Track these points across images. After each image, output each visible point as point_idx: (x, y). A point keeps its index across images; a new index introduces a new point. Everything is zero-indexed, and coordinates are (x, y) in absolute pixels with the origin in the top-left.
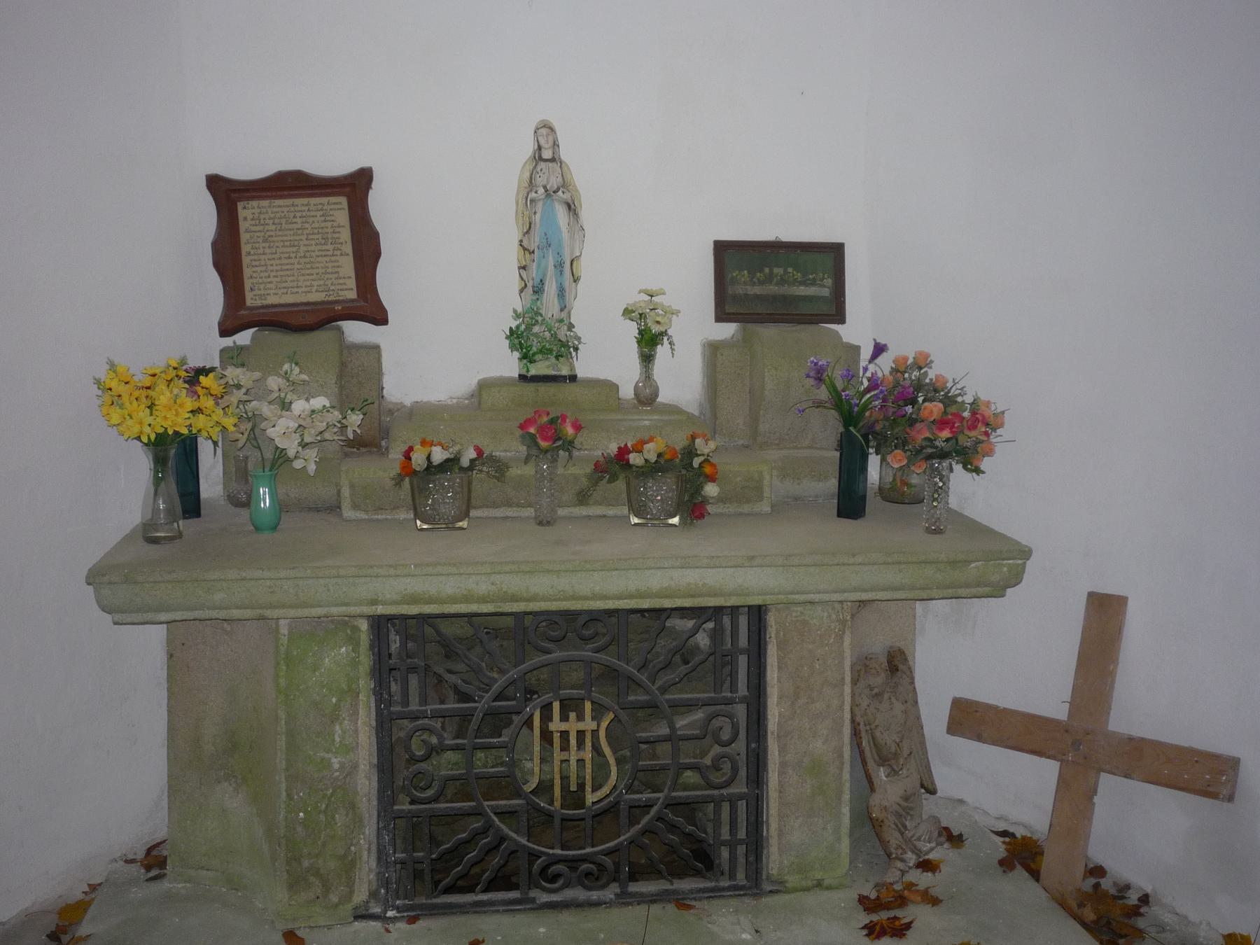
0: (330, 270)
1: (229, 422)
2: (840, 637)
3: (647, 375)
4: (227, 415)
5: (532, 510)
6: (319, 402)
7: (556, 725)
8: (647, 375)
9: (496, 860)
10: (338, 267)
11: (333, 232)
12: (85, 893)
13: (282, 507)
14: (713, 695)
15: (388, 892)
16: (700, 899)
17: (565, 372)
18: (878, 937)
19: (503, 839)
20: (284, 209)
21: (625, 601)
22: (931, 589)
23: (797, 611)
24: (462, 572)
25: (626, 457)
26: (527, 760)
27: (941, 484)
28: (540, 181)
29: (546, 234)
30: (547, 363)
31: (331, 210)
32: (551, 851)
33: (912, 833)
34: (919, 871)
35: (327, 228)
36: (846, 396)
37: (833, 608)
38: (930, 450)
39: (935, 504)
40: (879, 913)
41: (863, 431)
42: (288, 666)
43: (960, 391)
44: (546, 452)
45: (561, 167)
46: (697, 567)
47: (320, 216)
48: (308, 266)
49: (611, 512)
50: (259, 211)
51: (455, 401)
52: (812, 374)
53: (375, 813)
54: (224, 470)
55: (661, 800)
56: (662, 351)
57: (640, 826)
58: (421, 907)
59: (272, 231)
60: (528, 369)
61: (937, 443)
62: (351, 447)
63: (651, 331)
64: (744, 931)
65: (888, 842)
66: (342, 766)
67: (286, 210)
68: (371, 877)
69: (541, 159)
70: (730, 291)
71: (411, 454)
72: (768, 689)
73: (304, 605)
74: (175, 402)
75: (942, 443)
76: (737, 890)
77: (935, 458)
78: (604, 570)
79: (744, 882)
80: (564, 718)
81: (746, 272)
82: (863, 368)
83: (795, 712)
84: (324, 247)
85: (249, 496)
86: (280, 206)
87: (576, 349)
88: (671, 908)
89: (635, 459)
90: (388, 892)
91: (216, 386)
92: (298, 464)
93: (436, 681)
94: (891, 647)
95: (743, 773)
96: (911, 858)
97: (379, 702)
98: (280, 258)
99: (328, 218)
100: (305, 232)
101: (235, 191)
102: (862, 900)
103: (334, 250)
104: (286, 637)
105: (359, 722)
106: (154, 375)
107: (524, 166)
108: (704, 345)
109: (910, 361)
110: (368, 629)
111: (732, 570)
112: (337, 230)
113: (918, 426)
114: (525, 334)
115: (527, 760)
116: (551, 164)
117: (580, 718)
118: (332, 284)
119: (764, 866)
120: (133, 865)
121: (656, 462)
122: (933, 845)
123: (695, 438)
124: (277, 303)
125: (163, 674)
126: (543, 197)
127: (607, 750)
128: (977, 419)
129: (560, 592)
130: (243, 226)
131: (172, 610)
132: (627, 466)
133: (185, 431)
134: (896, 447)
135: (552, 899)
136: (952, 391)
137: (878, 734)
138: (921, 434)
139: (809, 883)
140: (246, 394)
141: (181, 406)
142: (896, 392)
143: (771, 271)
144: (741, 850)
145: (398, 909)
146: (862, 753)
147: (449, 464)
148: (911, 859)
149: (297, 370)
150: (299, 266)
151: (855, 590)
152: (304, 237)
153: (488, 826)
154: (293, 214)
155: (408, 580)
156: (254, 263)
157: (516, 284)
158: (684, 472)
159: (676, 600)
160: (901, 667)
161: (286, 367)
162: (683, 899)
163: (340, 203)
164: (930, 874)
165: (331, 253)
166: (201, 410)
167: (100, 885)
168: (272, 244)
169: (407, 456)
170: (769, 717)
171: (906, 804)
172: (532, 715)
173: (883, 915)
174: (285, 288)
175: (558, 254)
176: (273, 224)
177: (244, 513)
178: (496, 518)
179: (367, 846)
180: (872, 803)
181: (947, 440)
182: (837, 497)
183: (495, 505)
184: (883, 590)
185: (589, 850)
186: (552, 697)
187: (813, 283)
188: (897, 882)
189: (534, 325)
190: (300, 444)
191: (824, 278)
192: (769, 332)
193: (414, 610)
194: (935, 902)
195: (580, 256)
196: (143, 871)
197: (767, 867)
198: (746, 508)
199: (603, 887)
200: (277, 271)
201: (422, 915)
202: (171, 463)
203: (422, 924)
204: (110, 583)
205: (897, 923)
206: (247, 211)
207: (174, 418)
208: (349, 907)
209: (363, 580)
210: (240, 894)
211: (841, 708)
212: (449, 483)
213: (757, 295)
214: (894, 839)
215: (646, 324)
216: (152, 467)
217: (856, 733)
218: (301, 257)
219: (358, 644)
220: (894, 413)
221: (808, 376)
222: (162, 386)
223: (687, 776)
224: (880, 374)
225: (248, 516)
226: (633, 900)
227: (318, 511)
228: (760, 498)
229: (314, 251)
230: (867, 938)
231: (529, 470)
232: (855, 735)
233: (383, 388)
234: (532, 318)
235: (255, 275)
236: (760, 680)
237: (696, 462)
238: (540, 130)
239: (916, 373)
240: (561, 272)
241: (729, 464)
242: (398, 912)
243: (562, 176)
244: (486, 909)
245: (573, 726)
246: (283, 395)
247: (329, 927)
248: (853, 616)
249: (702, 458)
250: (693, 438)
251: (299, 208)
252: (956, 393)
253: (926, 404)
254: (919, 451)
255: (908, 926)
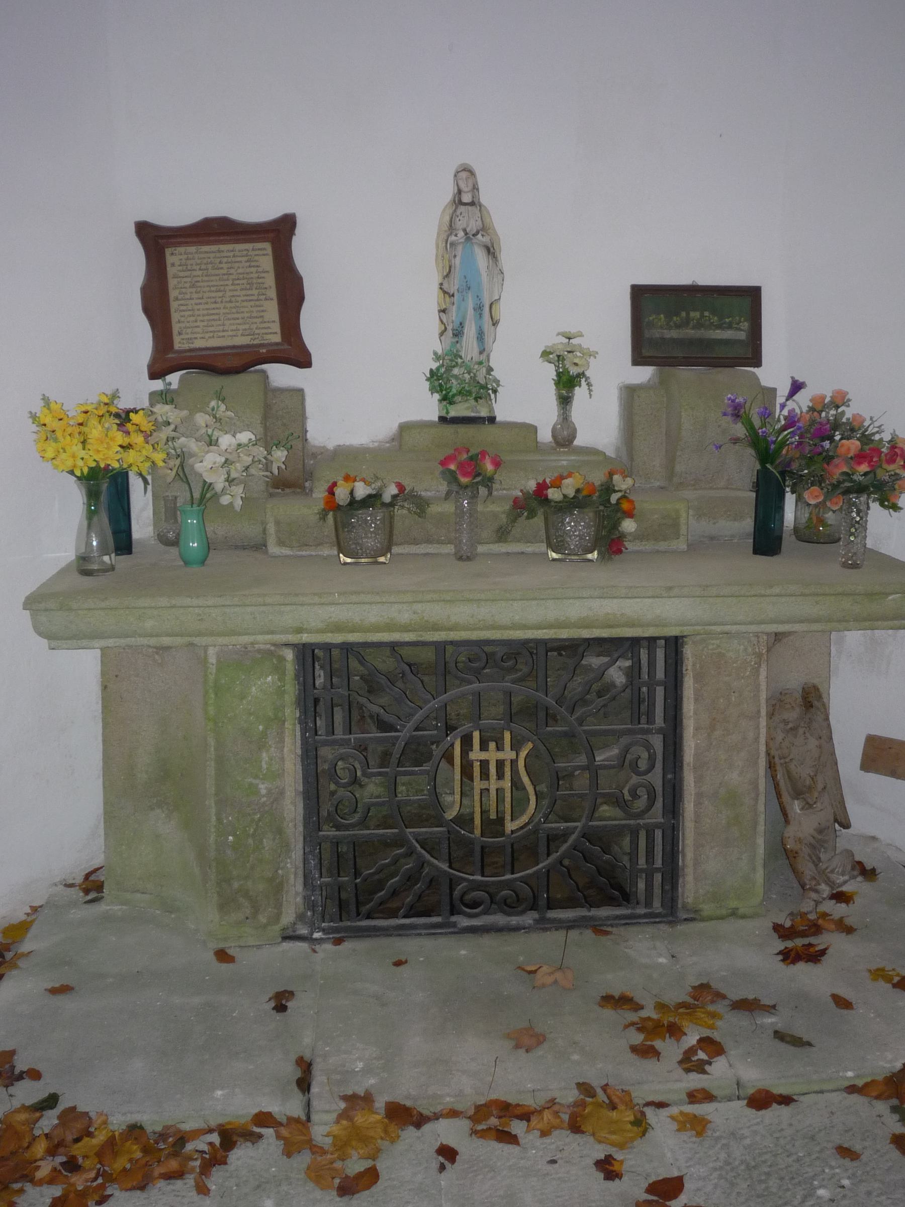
0: (255, 314)
1: (159, 457)
2: (756, 671)
3: (565, 416)
4: (156, 450)
5: (452, 547)
6: (245, 437)
7: (476, 755)
8: (565, 416)
9: (418, 885)
10: (263, 311)
11: (258, 278)
12: (28, 914)
13: (209, 546)
14: (630, 726)
15: (314, 915)
16: (617, 925)
17: (484, 413)
18: (794, 962)
19: (422, 864)
20: (209, 255)
21: (544, 631)
22: (847, 621)
23: (713, 644)
24: (384, 600)
25: (545, 492)
26: (447, 793)
27: (858, 519)
28: (460, 224)
29: (465, 277)
30: (467, 405)
31: (256, 255)
32: (471, 878)
33: (826, 865)
34: (834, 901)
35: (252, 273)
36: (763, 432)
37: (750, 641)
38: (848, 484)
39: (852, 539)
40: (794, 941)
41: (780, 469)
42: (216, 694)
43: (877, 429)
44: (466, 487)
45: (480, 210)
46: (615, 598)
47: (246, 262)
48: (234, 310)
49: (530, 548)
50: (186, 256)
51: (376, 444)
52: (730, 410)
53: (301, 838)
54: (154, 510)
55: (578, 829)
56: (580, 393)
57: (558, 854)
58: (345, 929)
59: (198, 276)
60: (447, 410)
61: (855, 477)
62: (275, 488)
63: (569, 372)
64: (660, 955)
65: (802, 873)
66: (269, 791)
67: (212, 255)
68: (298, 899)
69: (461, 203)
70: (647, 334)
71: (335, 489)
72: (685, 721)
73: (233, 633)
74: (107, 435)
75: (861, 478)
76: (653, 918)
77: (852, 493)
78: (523, 600)
79: (660, 910)
80: (484, 747)
81: (662, 316)
82: (781, 405)
83: (711, 744)
84: (250, 292)
85: (178, 536)
86: (206, 252)
87: (495, 391)
88: (588, 934)
89: (554, 494)
90: (314, 915)
91: (146, 422)
92: (225, 500)
93: (359, 717)
94: (806, 684)
95: (659, 804)
96: (825, 890)
97: (304, 731)
98: (207, 303)
99: (253, 264)
100: (231, 277)
101: (163, 237)
102: (777, 928)
103: (259, 295)
104: (214, 667)
105: (286, 750)
106: (86, 412)
107: (444, 210)
108: (621, 389)
109: (827, 400)
110: (293, 659)
111: (650, 600)
112: (263, 275)
113: (836, 461)
114: (445, 376)
115: (447, 793)
116: (470, 208)
117: (499, 748)
118: (256, 328)
119: (680, 894)
120: (72, 889)
121: (574, 497)
122: (846, 878)
123: (613, 475)
124: (203, 346)
125: (97, 708)
126: (463, 240)
127: (526, 780)
128: (896, 454)
129: (480, 621)
130: (171, 271)
131: (106, 638)
132: (546, 501)
133: (116, 465)
134: (813, 484)
135: (472, 924)
136: (870, 429)
137: (792, 767)
138: (838, 470)
139: (724, 912)
140: (175, 430)
141: (113, 439)
142: (812, 430)
143: (688, 314)
144: (658, 877)
145: (323, 930)
146: (776, 786)
147: (372, 499)
148: (824, 890)
149: (223, 407)
150: (225, 311)
151: (772, 621)
152: (230, 282)
153: (411, 853)
154: (219, 260)
155: (332, 609)
156: (182, 308)
157: (436, 327)
158: (601, 508)
159: (594, 630)
160: (816, 703)
161: (213, 403)
162: (601, 925)
163: (264, 249)
164: (843, 905)
165: (255, 298)
166: (131, 446)
167: (40, 907)
168: (199, 289)
169: (331, 492)
170: (685, 748)
171: (820, 837)
172: (452, 745)
173: (799, 942)
174: (211, 332)
175: (478, 296)
176: (200, 269)
177: (174, 551)
178: (418, 555)
179: (293, 870)
180: (786, 835)
181: (865, 474)
182: (752, 537)
183: (415, 542)
184: (801, 622)
185: (508, 876)
186: (472, 726)
187: (730, 327)
188: (811, 912)
189: (454, 367)
190: (227, 480)
191: (740, 322)
192: (685, 373)
193: (338, 638)
194: (849, 930)
195: (499, 299)
196: (82, 894)
197: (683, 896)
198: (662, 546)
199: (523, 912)
200: (204, 315)
201: (346, 937)
202: (103, 498)
203: (347, 945)
204: (46, 610)
205: (811, 950)
206: (175, 258)
207: (106, 451)
208: (277, 928)
209: (288, 608)
210: (173, 916)
211: (757, 739)
212: (373, 518)
213: (674, 339)
214: (808, 870)
215: (564, 366)
216: (85, 502)
217: (771, 766)
218: (226, 302)
219: (284, 674)
220: (810, 451)
221: (725, 414)
222: (94, 422)
223: (603, 811)
224: (798, 411)
225: (178, 553)
226: (551, 926)
227: (244, 549)
228: (677, 536)
229: (239, 296)
230: (782, 963)
231: (449, 507)
232: (770, 767)
233: (306, 431)
234: (451, 360)
235: (182, 319)
236: (676, 712)
237: (614, 498)
238: (460, 174)
239: (833, 412)
240: (481, 315)
241: (643, 503)
242: (324, 934)
243: (482, 219)
244: (408, 932)
245: (492, 755)
246: (210, 431)
247: (259, 947)
248: (768, 651)
249: (619, 495)
250: (611, 474)
251: (225, 254)
252: (873, 431)
253: (844, 441)
254: (835, 487)
255: (823, 952)
